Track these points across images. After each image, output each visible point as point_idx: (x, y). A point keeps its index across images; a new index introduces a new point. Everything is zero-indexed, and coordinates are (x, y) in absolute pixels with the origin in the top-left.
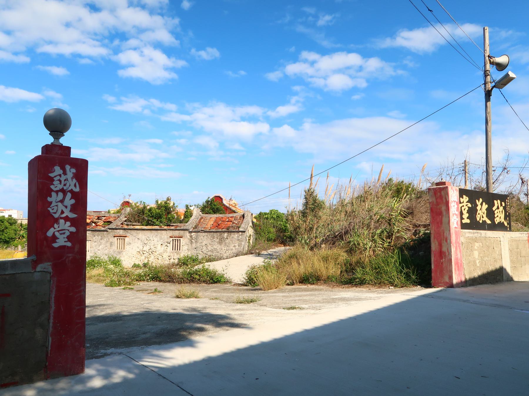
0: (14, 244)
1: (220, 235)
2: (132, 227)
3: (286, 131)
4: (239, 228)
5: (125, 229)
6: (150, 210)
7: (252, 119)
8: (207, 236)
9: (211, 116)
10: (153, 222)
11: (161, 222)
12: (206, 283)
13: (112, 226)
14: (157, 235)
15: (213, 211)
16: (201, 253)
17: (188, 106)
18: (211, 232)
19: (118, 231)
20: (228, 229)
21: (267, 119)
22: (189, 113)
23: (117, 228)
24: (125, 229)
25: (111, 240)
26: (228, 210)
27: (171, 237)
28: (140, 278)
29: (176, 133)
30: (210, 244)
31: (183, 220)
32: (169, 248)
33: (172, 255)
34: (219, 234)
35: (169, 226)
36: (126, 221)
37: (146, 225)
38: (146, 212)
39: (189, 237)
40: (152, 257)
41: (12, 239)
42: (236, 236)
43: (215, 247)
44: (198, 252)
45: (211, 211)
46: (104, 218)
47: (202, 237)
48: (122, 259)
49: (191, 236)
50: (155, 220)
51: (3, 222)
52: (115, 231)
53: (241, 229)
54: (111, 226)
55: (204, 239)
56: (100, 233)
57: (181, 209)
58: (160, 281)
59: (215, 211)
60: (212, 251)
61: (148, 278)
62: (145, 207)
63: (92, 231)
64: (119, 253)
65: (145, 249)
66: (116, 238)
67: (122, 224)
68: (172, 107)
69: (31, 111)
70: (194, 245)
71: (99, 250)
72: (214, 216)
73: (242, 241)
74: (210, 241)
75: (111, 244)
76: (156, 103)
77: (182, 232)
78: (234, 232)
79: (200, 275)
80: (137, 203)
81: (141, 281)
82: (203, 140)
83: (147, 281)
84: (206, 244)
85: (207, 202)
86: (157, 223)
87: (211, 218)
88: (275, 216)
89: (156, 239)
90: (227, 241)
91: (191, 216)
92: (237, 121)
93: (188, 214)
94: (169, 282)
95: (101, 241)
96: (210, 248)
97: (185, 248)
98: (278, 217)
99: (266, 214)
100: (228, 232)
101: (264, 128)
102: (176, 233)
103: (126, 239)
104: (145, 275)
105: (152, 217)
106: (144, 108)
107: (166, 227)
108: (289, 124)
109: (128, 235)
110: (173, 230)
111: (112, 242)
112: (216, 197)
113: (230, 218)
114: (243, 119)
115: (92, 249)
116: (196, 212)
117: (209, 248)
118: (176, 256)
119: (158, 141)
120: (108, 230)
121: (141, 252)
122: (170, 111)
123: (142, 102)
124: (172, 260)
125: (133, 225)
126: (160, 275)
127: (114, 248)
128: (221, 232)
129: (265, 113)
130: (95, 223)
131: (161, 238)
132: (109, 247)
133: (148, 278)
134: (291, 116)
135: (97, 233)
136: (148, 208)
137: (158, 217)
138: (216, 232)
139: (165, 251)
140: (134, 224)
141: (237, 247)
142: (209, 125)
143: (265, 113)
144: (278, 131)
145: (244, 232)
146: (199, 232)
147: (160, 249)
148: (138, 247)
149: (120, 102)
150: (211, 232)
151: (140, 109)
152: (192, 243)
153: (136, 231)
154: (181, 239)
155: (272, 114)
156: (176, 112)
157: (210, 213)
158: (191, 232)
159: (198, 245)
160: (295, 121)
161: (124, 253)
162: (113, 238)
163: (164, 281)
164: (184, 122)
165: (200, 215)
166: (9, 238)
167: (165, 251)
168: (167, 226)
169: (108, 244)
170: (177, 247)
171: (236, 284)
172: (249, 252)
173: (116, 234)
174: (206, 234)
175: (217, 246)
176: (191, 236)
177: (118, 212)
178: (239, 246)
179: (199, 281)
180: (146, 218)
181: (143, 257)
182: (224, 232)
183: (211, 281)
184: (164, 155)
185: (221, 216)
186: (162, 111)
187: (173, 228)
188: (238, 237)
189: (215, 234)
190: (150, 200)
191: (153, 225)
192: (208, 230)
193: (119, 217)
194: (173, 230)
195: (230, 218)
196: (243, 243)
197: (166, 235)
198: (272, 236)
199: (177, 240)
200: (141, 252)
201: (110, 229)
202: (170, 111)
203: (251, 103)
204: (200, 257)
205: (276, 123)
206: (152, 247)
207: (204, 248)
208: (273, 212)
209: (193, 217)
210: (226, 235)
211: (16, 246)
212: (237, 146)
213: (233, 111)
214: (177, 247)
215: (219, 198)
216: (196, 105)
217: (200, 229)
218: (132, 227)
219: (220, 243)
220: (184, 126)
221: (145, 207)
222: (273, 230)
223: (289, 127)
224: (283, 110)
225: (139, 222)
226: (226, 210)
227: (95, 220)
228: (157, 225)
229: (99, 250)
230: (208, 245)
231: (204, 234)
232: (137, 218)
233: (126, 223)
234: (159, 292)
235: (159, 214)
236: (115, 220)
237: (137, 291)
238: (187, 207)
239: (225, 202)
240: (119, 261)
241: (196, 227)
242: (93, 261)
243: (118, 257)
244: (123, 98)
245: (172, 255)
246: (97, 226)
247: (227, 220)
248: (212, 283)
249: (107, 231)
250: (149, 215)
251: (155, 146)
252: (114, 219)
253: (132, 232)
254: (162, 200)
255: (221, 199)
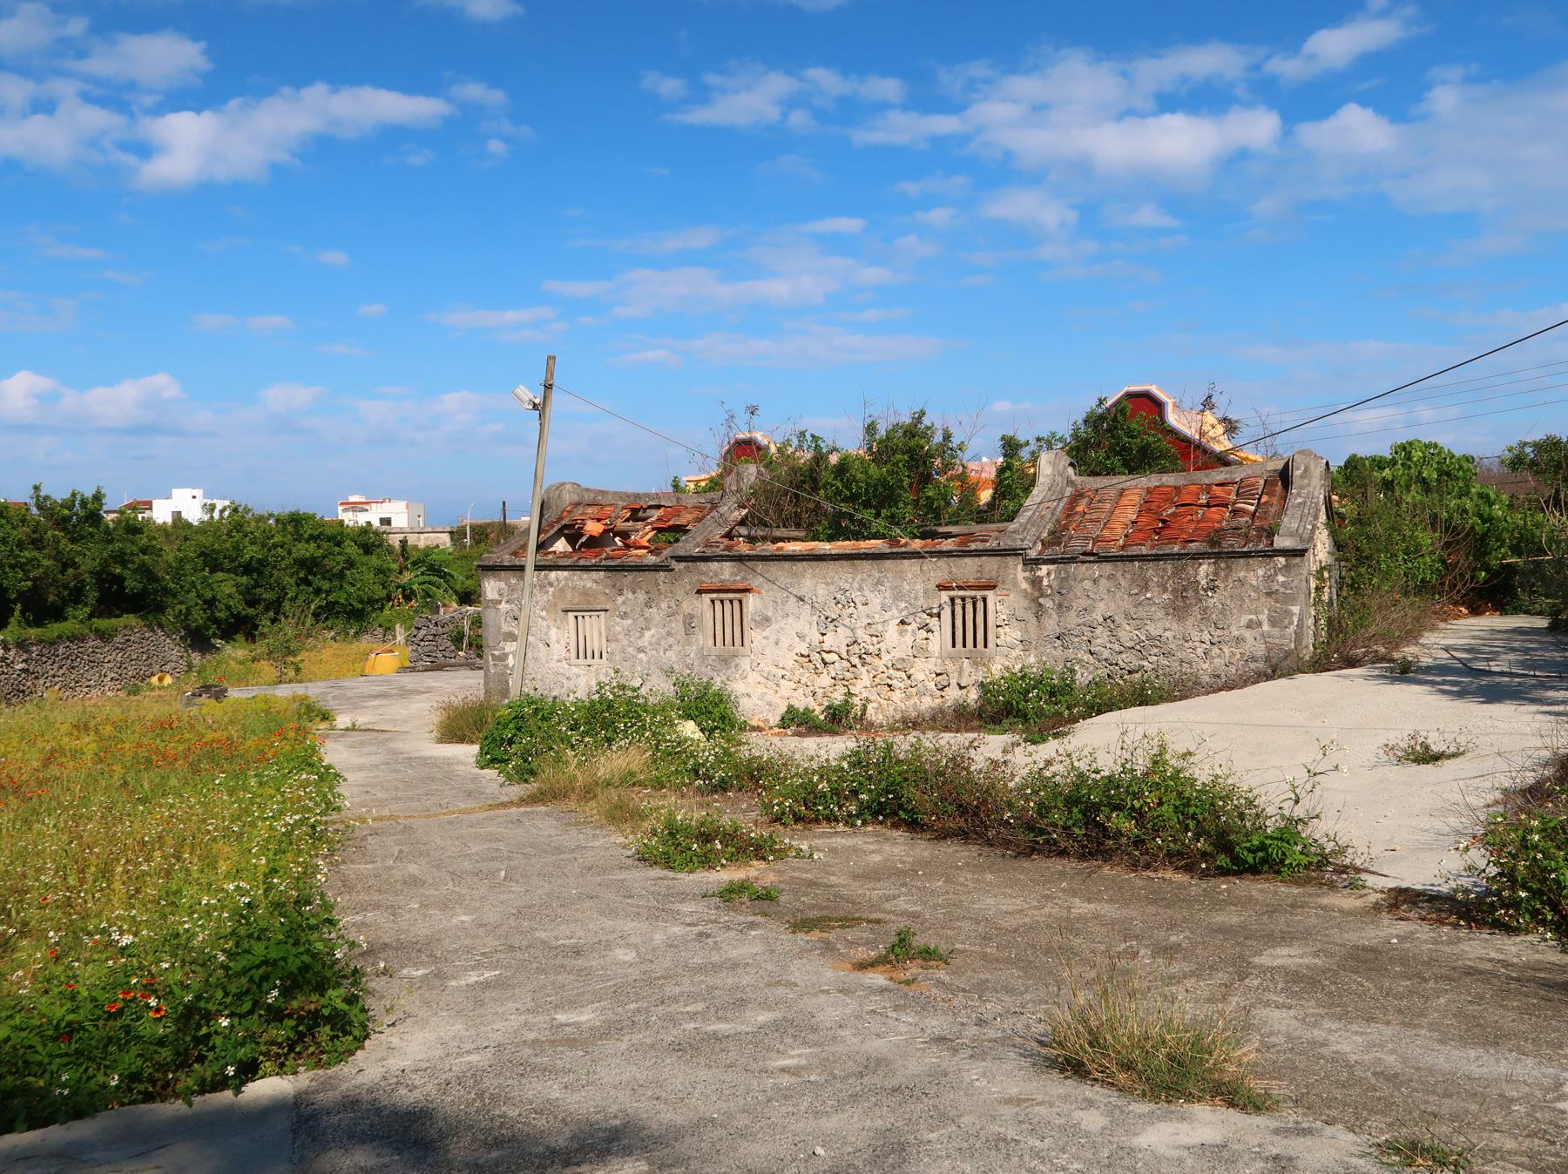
0: (381, 619)
1: (1178, 572)
2: (770, 548)
3: (1359, 130)
4: (1271, 534)
5: (740, 559)
6: (842, 469)
7: (1203, 99)
8: (1111, 577)
9: (1040, 108)
10: (860, 522)
11: (893, 520)
12: (1189, 869)
13: (688, 546)
14: (879, 582)
15: (1126, 464)
16: (1087, 657)
17: (949, 80)
18: (1132, 559)
19: (715, 566)
20: (1213, 543)
21: (1266, 91)
22: (956, 109)
23: (709, 552)
24: (740, 559)
25: (686, 607)
26: (1190, 452)
27: (942, 587)
28: (814, 805)
29: (911, 188)
30: (1128, 617)
31: (991, 505)
32: (935, 639)
33: (950, 667)
34: (1169, 567)
35: (932, 535)
36: (742, 523)
37: (830, 539)
38: (826, 476)
39: (1024, 585)
40: (866, 679)
41: (371, 601)
42: (1254, 574)
43: (1155, 630)
44: (1070, 653)
45: (1117, 461)
46: (656, 514)
47: (1087, 584)
48: (738, 687)
49: (1036, 582)
50: (867, 515)
51: (338, 544)
52: (702, 566)
53: (1281, 542)
54: (688, 546)
55: (1101, 595)
56: (640, 577)
57: (983, 463)
58: (914, 825)
59: (1138, 460)
60: (1139, 649)
61: (853, 809)
62: (820, 458)
63: (608, 569)
64: (726, 661)
65: (830, 641)
66: (707, 597)
67: (728, 536)
68: (889, 88)
69: (417, 161)
70: (1051, 624)
71: (641, 650)
72: (1138, 485)
73: (1291, 599)
74: (1127, 604)
75: (690, 625)
76: (826, 80)
77: (991, 564)
78: (1247, 555)
79: (1139, 816)
80: (788, 443)
81: (816, 821)
82: (1018, 205)
83: (849, 820)
84: (1111, 616)
85: (1094, 421)
86: (879, 525)
87: (1122, 493)
88: (1430, 473)
89: (876, 601)
90: (1214, 600)
91: (1027, 490)
92: (1143, 115)
93: (1013, 483)
94: (963, 835)
95: (648, 612)
96: (1127, 633)
97: (1011, 635)
98: (1445, 474)
99: (1379, 463)
100: (1218, 556)
101: (1258, 127)
102: (968, 569)
103: (751, 601)
104: (835, 792)
105: (852, 499)
106: (789, 103)
107: (917, 544)
108: (1364, 101)
109: (755, 582)
110: (948, 554)
111: (691, 617)
112: (1131, 396)
113: (1218, 491)
114: (1167, 103)
115: (613, 646)
116: (1050, 469)
117: (1122, 635)
118: (972, 675)
119: (850, 225)
120: (674, 564)
121: (816, 657)
122: (884, 106)
123: (779, 84)
124: (953, 694)
125: (775, 540)
126: (912, 793)
127: (703, 639)
128: (1180, 556)
129: (1257, 67)
130: (625, 535)
131: (898, 596)
132: (681, 635)
133: (853, 809)
134: (1370, 62)
135: (630, 577)
136: (834, 459)
137: (882, 497)
138: (1157, 558)
139: (920, 651)
140: (777, 533)
141: (1266, 627)
142: (1034, 143)
143: (1257, 67)
144: (1316, 135)
145: (1301, 553)
146: (1073, 560)
147: (897, 642)
148: (801, 637)
149: (701, 95)
150: (1132, 559)
151: (773, 113)
152: (1039, 611)
153: (787, 565)
154: (990, 594)
155: (1286, 67)
156: (905, 108)
157: (1111, 472)
158: (1037, 562)
159: (1072, 620)
160: (1390, 84)
161: (745, 663)
162: (694, 598)
163: (943, 835)
164: (938, 141)
165: (1070, 483)
166: (361, 601)
167: (920, 651)
168: (924, 536)
169: (677, 625)
170: (971, 634)
171: (1403, 899)
172: (1334, 654)
173: (708, 582)
174: (1108, 568)
175: (1163, 626)
176: (1036, 582)
177: (715, 484)
178: (1273, 622)
179: (1140, 855)
180: (828, 507)
181: (825, 680)
182: (1198, 557)
183: (1223, 860)
184: (873, 274)
185: (1169, 479)
186: (852, 110)
187: (948, 545)
188: (1269, 579)
189: (1151, 570)
190: (837, 424)
191: (857, 536)
192: (1114, 551)
193: (714, 506)
194: (948, 554)
195: (1218, 491)
196: (1296, 609)
197: (918, 579)
198: (1426, 566)
199: (968, 603)
200: (816, 657)
201: (679, 559)
202: (884, 106)
203: (1197, 35)
204: (1083, 677)
205: (1307, 102)
206: (861, 635)
207: (1102, 636)
208: (1417, 455)
209: (1038, 493)
210: (1205, 569)
211: (389, 629)
212: (1148, 216)
213: (1124, 74)
214: (971, 634)
215: (1147, 403)
216: (978, 69)
217: (1077, 546)
218: (770, 548)
219: (1178, 609)
220: (942, 156)
221: (820, 458)
222: (1426, 538)
223: (1369, 113)
224: (1334, 45)
225: (798, 525)
226: (1185, 456)
227: (621, 525)
228: (875, 536)
229: (641, 650)
230: (1119, 619)
231: (1096, 570)
232: (789, 509)
233: (743, 531)
234: (928, 955)
235: (884, 483)
236: (698, 520)
237: (802, 925)
238: (1011, 447)
239: (1172, 419)
240: (720, 699)
241: (1055, 538)
242: (610, 707)
243: (717, 683)
244: (711, 79)
245: (950, 667)
246: (627, 546)
247: (1203, 499)
248: (1224, 872)
249: (667, 569)
250: (838, 492)
251: (836, 244)
252: (696, 514)
253: (774, 569)
254: (893, 414)
255: (1158, 406)
